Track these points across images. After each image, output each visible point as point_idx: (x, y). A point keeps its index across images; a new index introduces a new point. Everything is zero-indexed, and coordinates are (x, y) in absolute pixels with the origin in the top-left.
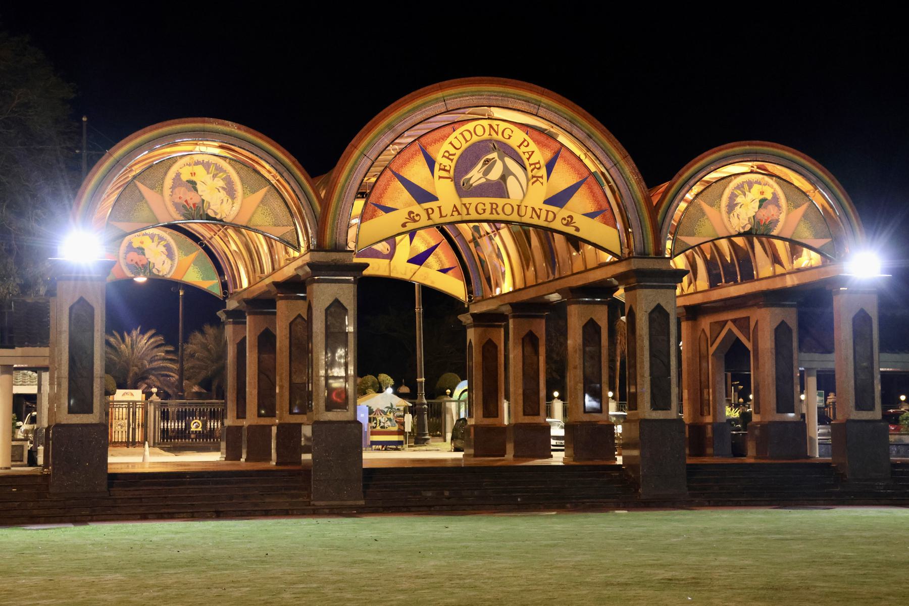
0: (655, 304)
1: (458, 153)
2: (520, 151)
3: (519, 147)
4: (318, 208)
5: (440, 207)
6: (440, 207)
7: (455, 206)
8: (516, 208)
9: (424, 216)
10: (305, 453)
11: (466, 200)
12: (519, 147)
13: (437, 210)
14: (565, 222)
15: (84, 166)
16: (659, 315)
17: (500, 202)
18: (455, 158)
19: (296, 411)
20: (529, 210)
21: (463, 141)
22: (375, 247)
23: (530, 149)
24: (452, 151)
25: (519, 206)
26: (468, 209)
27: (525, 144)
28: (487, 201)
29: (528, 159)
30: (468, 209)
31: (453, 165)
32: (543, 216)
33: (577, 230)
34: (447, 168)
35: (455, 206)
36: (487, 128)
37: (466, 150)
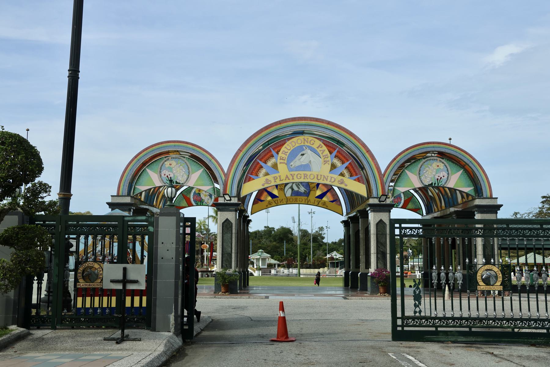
0: (379, 219)
1: (289, 151)
2: (318, 150)
4: (223, 178)
5: (280, 176)
7: (287, 176)
8: (316, 176)
9: (273, 181)
10: (48, 275)
11: (292, 173)
13: (278, 178)
15: (356, 177)
16: (380, 224)
17: (308, 173)
18: (288, 154)
19: (115, 261)
20: (322, 177)
22: (142, 187)
24: (286, 151)
25: (318, 175)
26: (293, 177)
28: (302, 173)
30: (293, 177)
31: (286, 157)
32: (329, 179)
33: (346, 185)
35: (287, 176)
36: (303, 140)
37: (293, 150)
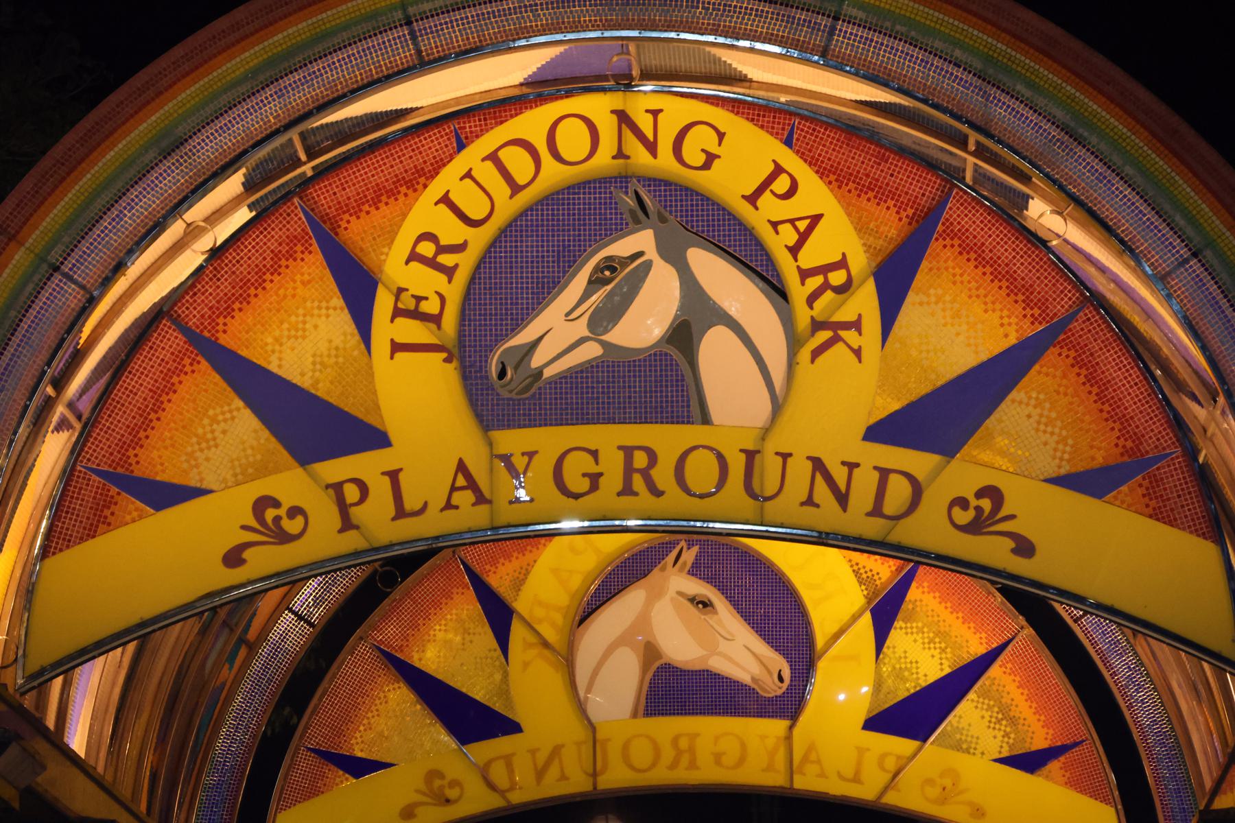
3: (752, 199)
6: (394, 476)
12: (752, 199)
14: (963, 517)
18: (465, 263)
21: (500, 189)
23: (798, 207)
24: (451, 230)
27: (781, 184)
29: (794, 250)
34: (431, 307)
